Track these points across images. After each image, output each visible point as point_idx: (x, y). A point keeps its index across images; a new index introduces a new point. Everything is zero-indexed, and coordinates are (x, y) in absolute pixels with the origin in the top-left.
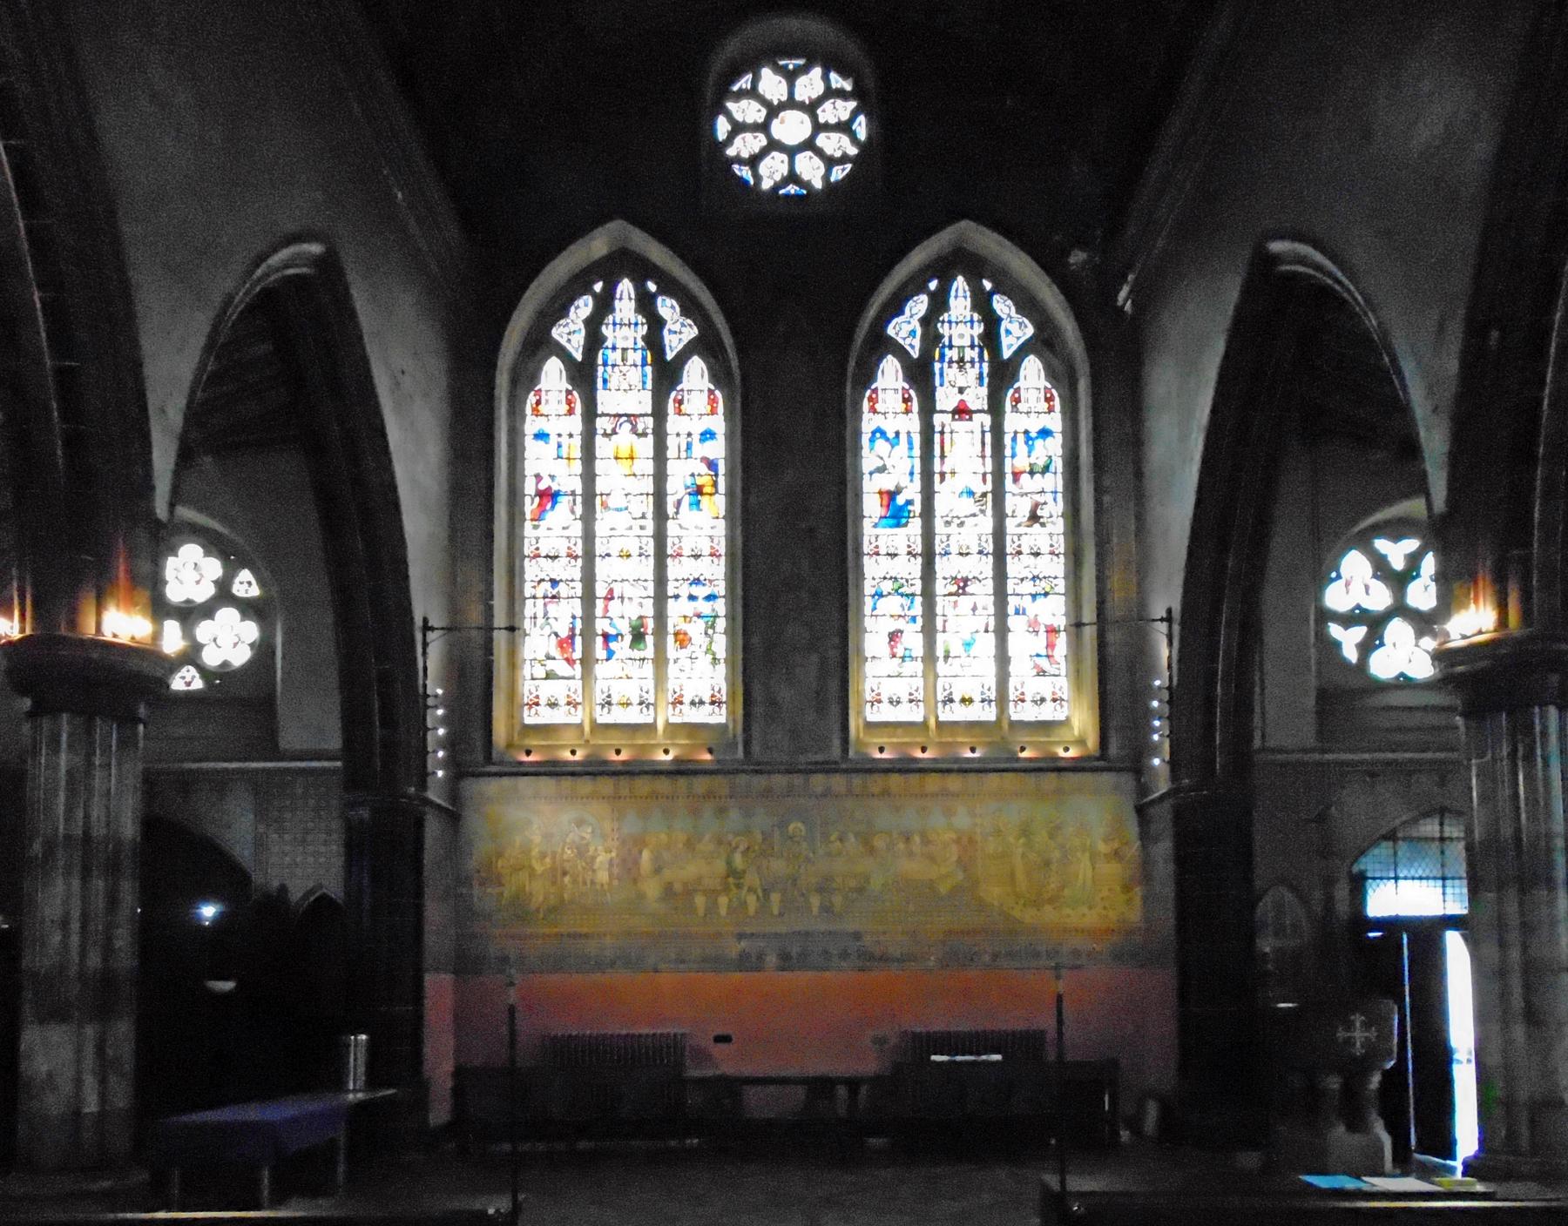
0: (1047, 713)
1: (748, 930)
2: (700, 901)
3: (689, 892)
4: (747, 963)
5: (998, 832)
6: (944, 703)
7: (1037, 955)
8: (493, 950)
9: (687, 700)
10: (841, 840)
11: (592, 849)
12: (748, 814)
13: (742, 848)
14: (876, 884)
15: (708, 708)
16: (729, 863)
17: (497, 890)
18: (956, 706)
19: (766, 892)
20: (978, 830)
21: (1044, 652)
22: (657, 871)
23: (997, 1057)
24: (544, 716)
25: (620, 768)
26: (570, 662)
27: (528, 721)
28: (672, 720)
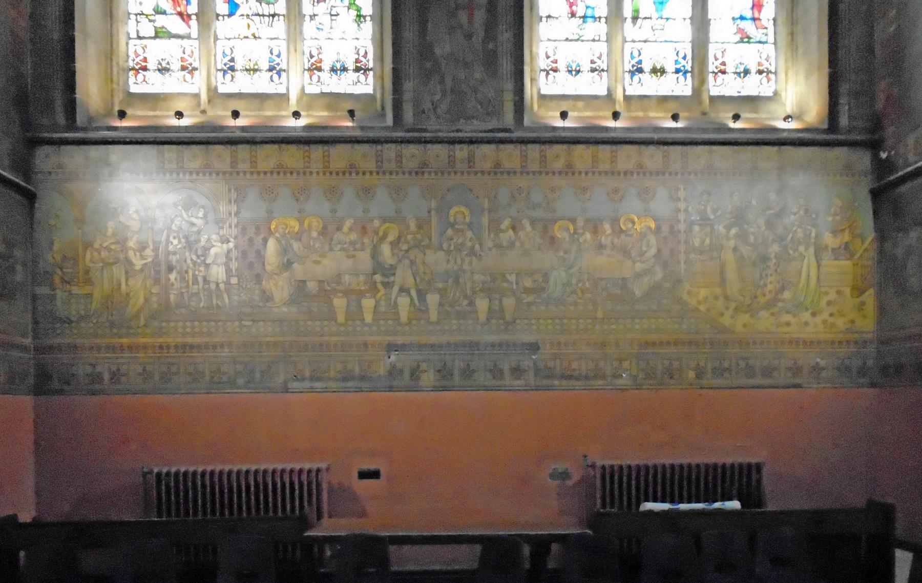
0: (752, 86)
1: (400, 340)
2: (339, 303)
3: (325, 293)
4: (402, 380)
5: (705, 221)
6: (632, 73)
7: (750, 371)
8: (82, 371)
9: (326, 66)
10: (514, 228)
11: (204, 238)
12: (398, 192)
13: (391, 238)
14: (558, 277)
15: (352, 76)
16: (375, 254)
17: (87, 289)
18: (646, 77)
19: (422, 295)
20: (682, 217)
21: (749, 14)
22: (287, 265)
23: (735, 505)
24: (153, 83)
25: (238, 134)
26: (184, 17)
27: (134, 89)
28: (308, 90)
